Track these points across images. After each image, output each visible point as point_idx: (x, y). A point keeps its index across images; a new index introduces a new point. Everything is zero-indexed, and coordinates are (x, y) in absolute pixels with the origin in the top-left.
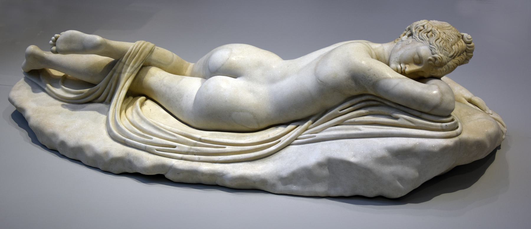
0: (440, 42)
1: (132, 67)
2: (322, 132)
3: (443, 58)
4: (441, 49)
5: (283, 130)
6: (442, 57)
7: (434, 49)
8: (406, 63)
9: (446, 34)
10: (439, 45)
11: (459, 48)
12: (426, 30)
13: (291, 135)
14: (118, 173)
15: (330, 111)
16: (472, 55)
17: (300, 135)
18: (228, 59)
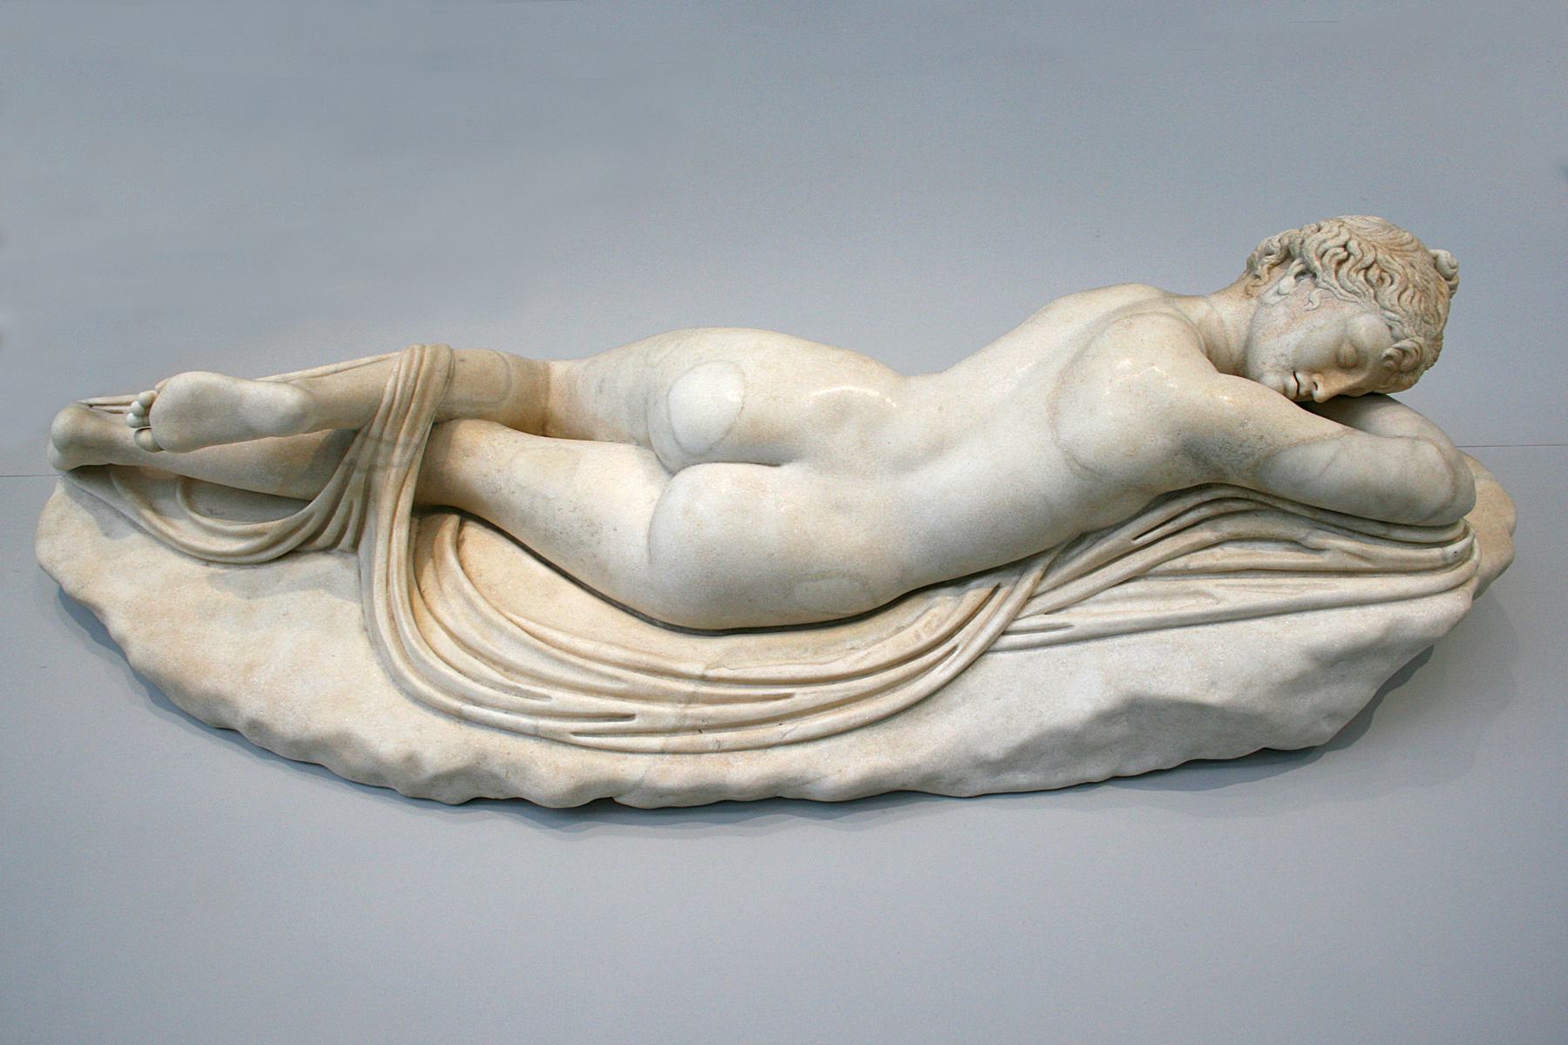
0: (1413, 298)
1: (407, 445)
4: (1418, 322)
5: (954, 610)
8: (1312, 370)
9: (1417, 268)
12: (1361, 260)
14: (455, 803)
17: (1014, 619)
18: (742, 408)
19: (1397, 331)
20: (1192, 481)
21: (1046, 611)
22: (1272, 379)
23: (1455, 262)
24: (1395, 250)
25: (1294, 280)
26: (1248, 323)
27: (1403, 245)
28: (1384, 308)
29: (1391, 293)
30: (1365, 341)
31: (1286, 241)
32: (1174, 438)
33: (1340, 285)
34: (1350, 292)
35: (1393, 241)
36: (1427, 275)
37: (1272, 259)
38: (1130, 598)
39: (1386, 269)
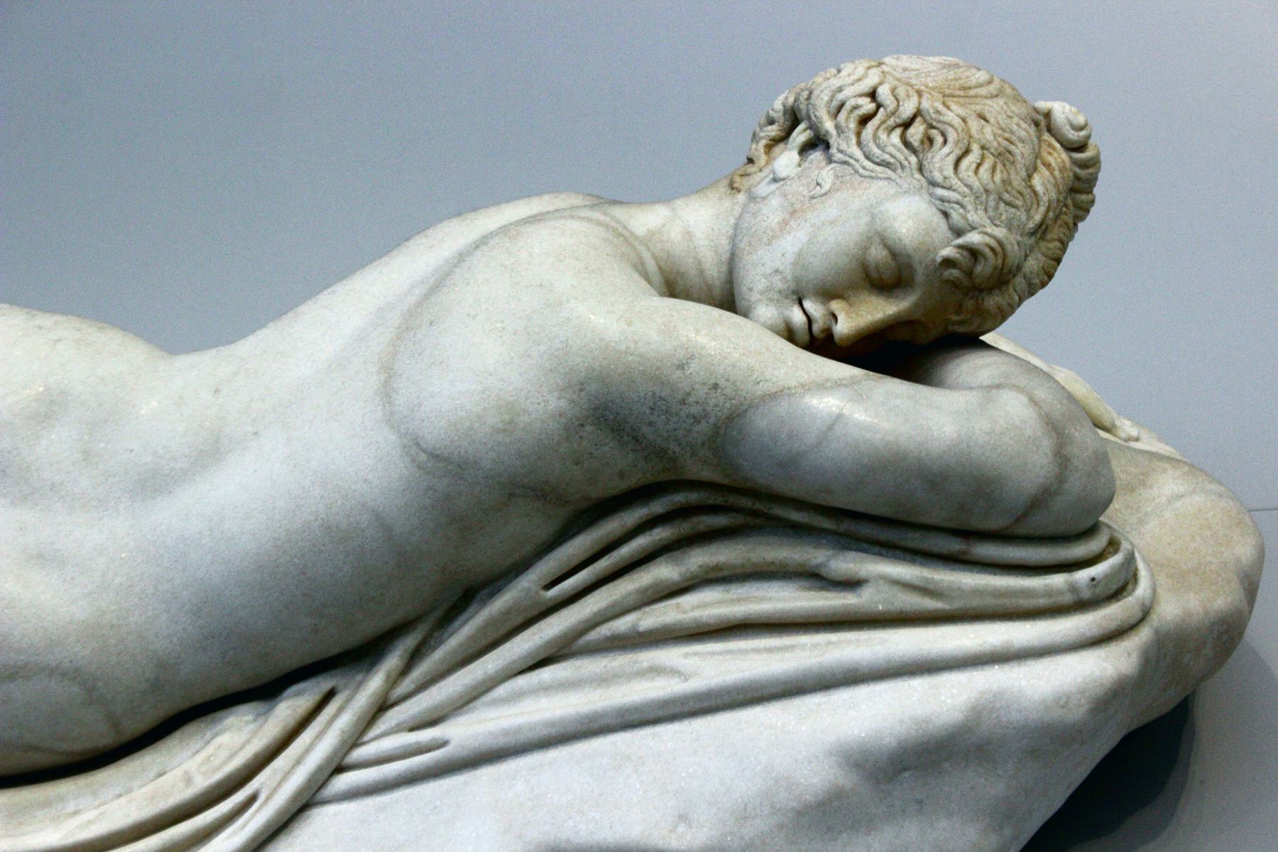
0: (979, 165)
2: (467, 712)
3: (1009, 247)
4: (992, 203)
6: (1005, 242)
7: (956, 206)
8: (828, 293)
9: (992, 120)
10: (976, 184)
11: (1055, 178)
12: (893, 113)
13: (307, 751)
15: (492, 595)
16: (1092, 202)
19: (956, 217)
20: (622, 475)
21: (409, 725)
22: (766, 312)
23: (1081, 120)
24: (954, 97)
27: (970, 88)
28: (933, 184)
29: (942, 159)
33: (865, 155)
34: (878, 164)
36: (1012, 132)
37: (773, 131)
38: (546, 689)
39: (934, 124)
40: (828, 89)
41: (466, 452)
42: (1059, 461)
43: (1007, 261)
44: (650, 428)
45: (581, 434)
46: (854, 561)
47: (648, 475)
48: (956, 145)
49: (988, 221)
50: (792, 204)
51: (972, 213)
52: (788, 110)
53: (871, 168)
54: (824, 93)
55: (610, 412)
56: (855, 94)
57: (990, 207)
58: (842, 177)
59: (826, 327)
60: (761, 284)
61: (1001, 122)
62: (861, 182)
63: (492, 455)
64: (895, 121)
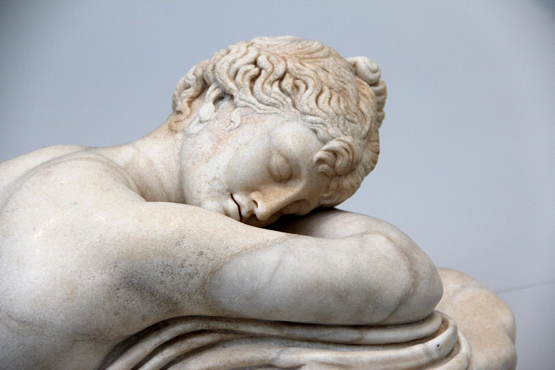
0: (330, 99)
3: (355, 147)
4: (341, 122)
6: (353, 144)
8: (249, 189)
9: (331, 71)
11: (370, 102)
12: (272, 72)
19: (322, 133)
20: (143, 318)
23: (374, 66)
24: (305, 59)
25: (213, 106)
26: (177, 157)
27: (313, 53)
28: (304, 113)
30: (292, 148)
31: (200, 72)
32: (112, 271)
33: (258, 100)
34: (268, 105)
35: (302, 50)
36: (343, 77)
37: (191, 92)
39: (298, 76)
40: (226, 62)
41: (44, 317)
42: (413, 274)
43: (355, 156)
44: (162, 285)
45: (118, 295)
46: (294, 353)
47: (160, 316)
48: (315, 88)
49: (341, 133)
50: (218, 136)
51: (331, 129)
52: (199, 78)
53: (264, 108)
54: (224, 65)
55: (135, 278)
56: (245, 63)
57: (341, 124)
58: (246, 115)
59: (250, 209)
60: (206, 188)
61: (336, 72)
62: (259, 117)
63: (62, 317)
64: (274, 77)
